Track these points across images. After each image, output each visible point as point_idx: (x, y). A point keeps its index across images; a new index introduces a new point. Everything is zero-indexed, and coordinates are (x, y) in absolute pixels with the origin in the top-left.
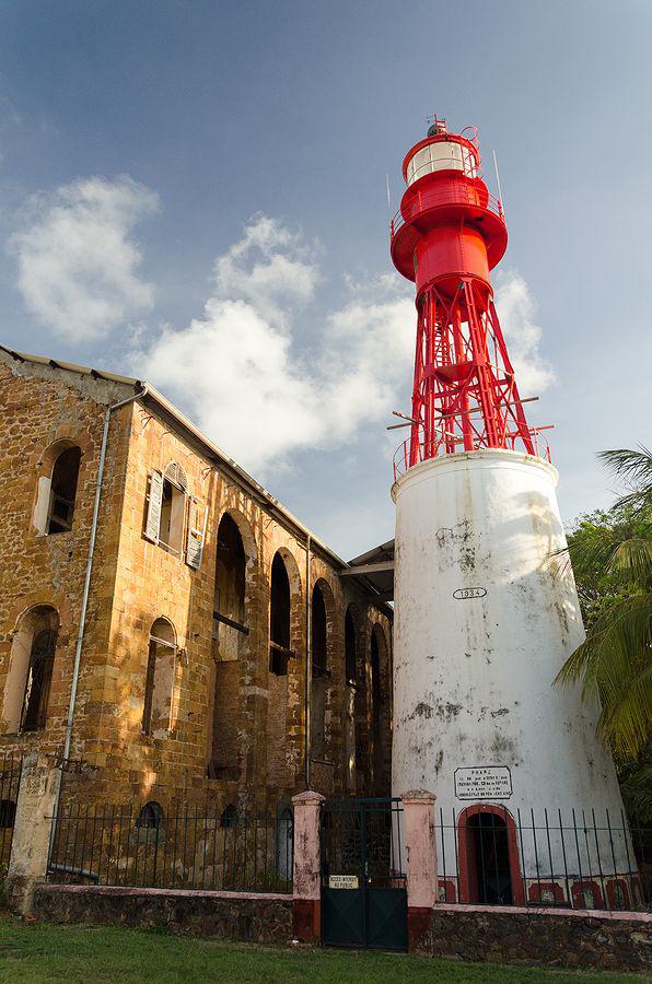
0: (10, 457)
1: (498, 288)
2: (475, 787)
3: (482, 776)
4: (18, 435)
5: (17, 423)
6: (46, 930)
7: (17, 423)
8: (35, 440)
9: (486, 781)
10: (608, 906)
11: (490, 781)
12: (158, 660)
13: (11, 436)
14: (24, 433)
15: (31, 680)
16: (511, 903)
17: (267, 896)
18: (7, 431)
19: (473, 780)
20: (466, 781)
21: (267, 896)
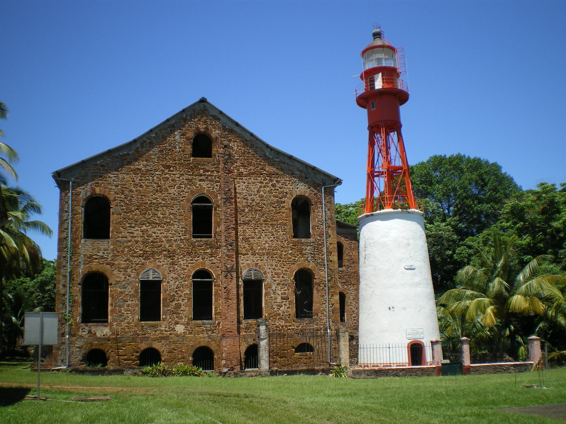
2: (413, 335)
5: (275, 182)
20: (410, 333)
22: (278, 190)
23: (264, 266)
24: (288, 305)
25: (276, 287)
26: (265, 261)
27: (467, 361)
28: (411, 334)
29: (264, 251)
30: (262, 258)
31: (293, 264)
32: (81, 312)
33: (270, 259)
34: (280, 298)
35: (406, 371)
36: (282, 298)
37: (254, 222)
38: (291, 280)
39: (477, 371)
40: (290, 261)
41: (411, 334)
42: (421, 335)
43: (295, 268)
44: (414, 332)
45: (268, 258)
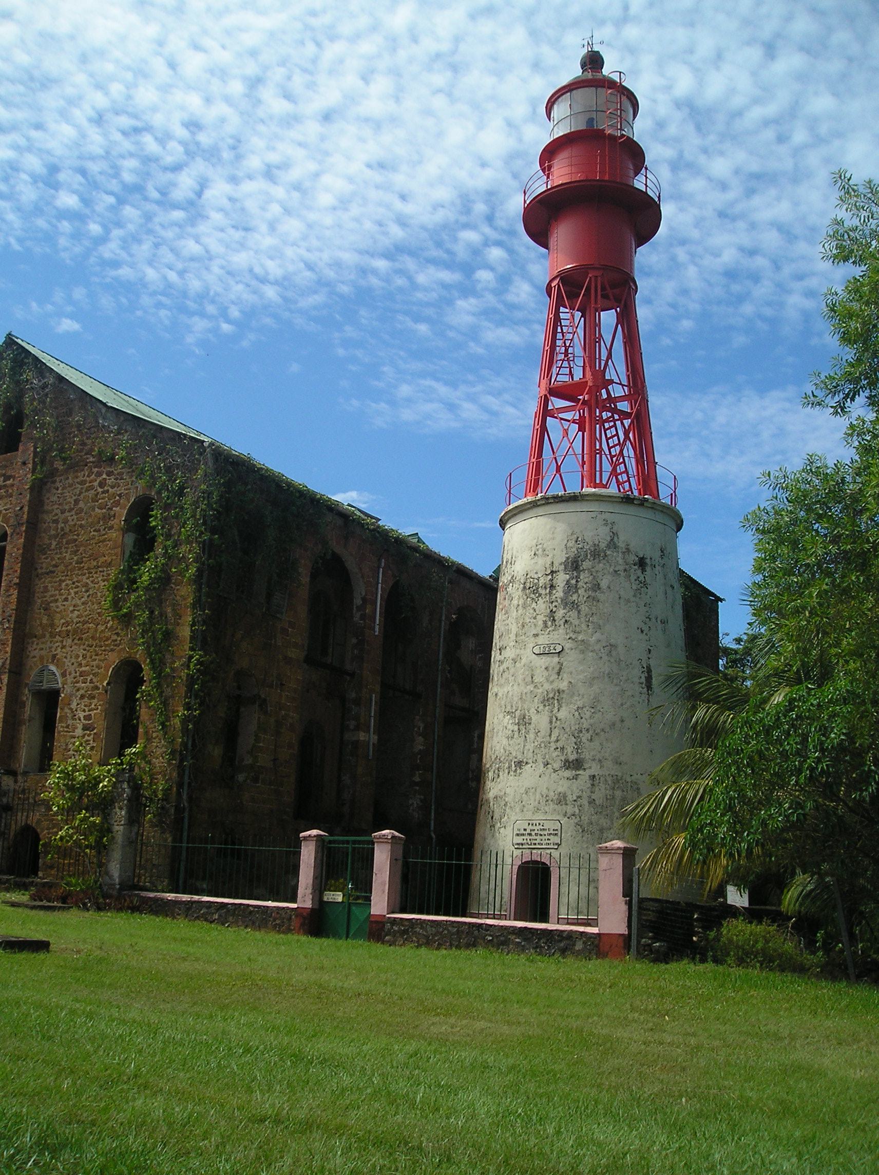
0: (100, 511)
1: (492, 196)
2: (529, 837)
3: (536, 828)
4: (106, 488)
5: (104, 476)
6: (769, 543)
7: (104, 476)
8: (120, 495)
9: (540, 832)
10: (851, 971)
11: (542, 833)
12: (242, 709)
13: (100, 490)
14: (112, 487)
15: (325, 859)
16: (464, 915)
17: (378, 613)
18: (96, 484)
19: (528, 831)
20: (522, 832)
21: (378, 613)
22: (108, 491)
23: (65, 660)
24: (91, 742)
25: (78, 704)
26: (68, 649)
27: (379, 904)
28: (523, 835)
29: (69, 628)
30: (64, 644)
31: (112, 650)
32: (21, 444)
33: (76, 644)
34: (80, 726)
35: (228, 911)
36: (85, 728)
37: (62, 567)
38: (103, 686)
39: (407, 932)
40: (106, 646)
41: (523, 835)
42: (551, 837)
43: (114, 659)
44: (534, 827)
45: (73, 640)
